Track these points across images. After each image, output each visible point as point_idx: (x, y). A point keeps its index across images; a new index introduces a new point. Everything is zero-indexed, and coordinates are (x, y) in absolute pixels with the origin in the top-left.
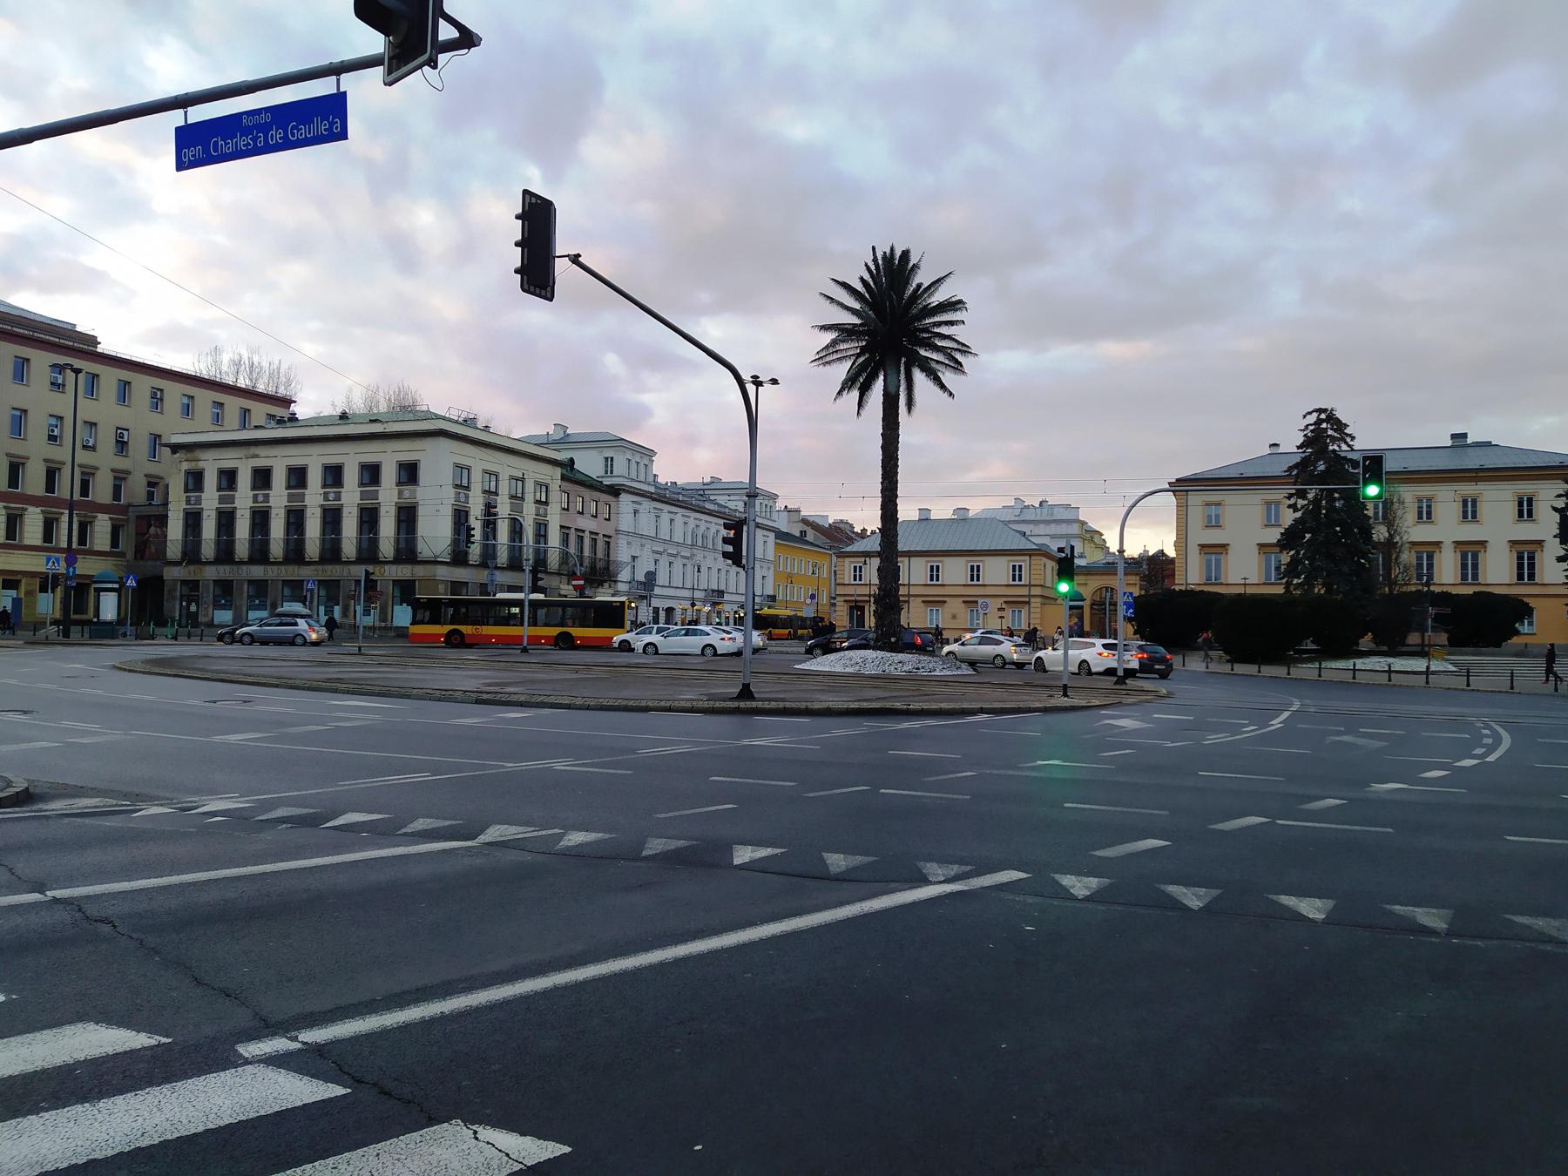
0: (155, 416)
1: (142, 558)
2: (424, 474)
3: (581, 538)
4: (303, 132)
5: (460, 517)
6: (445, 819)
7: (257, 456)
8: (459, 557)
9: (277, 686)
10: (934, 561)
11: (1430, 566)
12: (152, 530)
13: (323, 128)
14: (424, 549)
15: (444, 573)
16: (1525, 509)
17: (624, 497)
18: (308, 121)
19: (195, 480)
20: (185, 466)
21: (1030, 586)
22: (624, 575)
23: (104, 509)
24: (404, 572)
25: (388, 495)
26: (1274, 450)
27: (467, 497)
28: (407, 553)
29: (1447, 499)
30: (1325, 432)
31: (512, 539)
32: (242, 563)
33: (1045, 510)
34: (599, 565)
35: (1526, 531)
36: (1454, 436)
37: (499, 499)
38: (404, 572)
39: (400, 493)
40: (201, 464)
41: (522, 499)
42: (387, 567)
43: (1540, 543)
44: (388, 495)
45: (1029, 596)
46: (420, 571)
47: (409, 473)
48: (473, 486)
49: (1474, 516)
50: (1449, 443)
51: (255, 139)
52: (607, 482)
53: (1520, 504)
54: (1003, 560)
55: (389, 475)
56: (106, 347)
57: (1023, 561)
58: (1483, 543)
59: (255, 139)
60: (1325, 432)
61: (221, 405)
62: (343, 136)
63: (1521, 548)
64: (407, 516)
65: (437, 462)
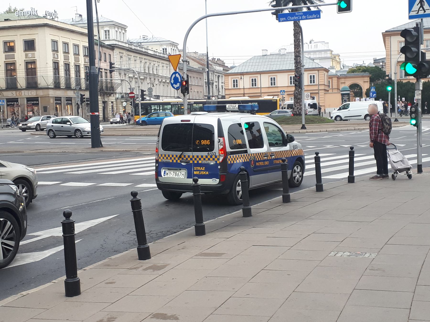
2: (37, 45)
3: (106, 73)
4: (310, 17)
5: (56, 65)
8: (57, 86)
9: (8, 152)
10: (273, 75)
13: (315, 16)
14: (41, 82)
15: (53, 93)
17: (116, 51)
18: (312, 15)
21: (319, 85)
22: (119, 90)
24: (32, 93)
27: (58, 55)
28: (32, 84)
31: (66, 74)
33: (313, 44)
34: (109, 85)
37: (70, 55)
38: (32, 93)
39: (26, 56)
41: (78, 54)
42: (23, 92)
44: (20, 57)
45: (318, 90)
46: (40, 93)
47: (30, 45)
48: (59, 50)
51: (299, 18)
52: (107, 43)
59: (299, 18)
62: (319, 18)
64: (31, 70)
65: (44, 39)
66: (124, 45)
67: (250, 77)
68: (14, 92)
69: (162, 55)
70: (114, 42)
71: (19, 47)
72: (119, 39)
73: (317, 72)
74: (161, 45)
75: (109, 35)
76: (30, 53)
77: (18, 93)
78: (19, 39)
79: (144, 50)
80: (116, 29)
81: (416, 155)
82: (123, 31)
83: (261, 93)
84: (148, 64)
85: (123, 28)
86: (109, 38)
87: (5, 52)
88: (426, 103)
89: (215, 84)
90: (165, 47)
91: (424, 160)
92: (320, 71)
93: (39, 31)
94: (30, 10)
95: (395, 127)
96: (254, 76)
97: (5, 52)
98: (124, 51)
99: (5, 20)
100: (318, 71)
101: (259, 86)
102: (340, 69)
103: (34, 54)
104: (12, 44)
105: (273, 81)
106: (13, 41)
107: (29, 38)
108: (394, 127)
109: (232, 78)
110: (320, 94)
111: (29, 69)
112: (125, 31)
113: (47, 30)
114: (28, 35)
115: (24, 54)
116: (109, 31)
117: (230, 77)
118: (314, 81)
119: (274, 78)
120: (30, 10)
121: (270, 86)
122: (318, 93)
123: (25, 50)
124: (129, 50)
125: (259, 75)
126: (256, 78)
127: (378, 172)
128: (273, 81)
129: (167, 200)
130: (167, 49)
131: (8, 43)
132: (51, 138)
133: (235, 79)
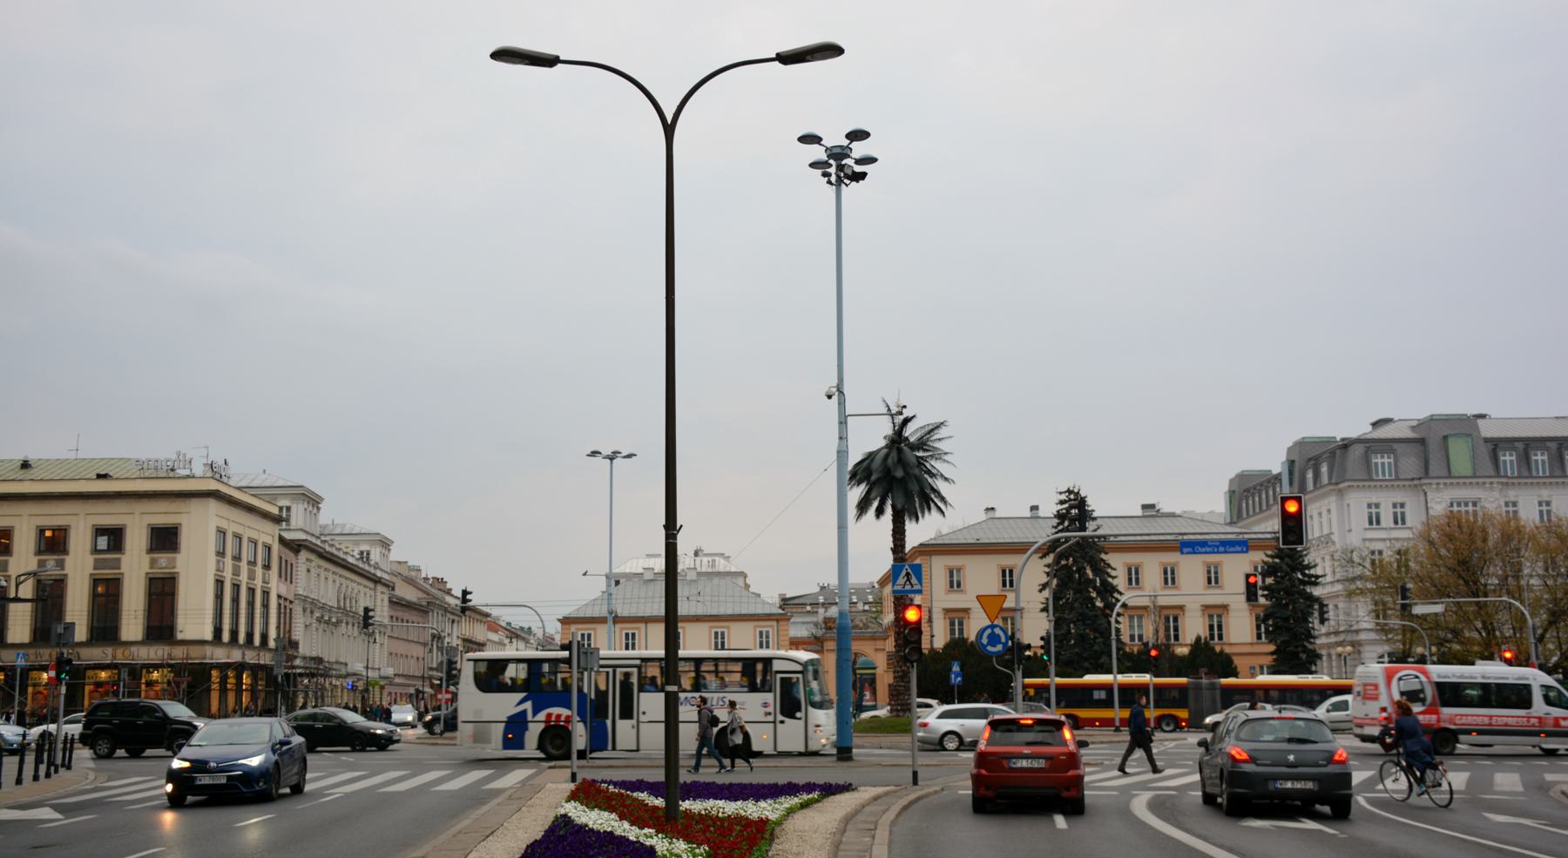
2: (185, 539)
5: (219, 583)
11: (1176, 629)
16: (1213, 579)
17: (304, 555)
26: (991, 514)
29: (1152, 567)
30: (1076, 510)
32: (81, 644)
35: (1214, 597)
36: (1144, 507)
39: (153, 563)
42: (134, 649)
43: (966, 611)
44: (135, 566)
47: (165, 539)
49: (1004, 572)
50: (1139, 512)
53: (1165, 572)
54: (705, 626)
55: (136, 540)
58: (1181, 608)
60: (1076, 510)
63: (953, 615)
64: (162, 593)
65: (201, 528)
68: (109, 651)
70: (302, 536)
71: (136, 540)
74: (357, 543)
76: (163, 558)
77: (119, 652)
78: (137, 524)
79: (341, 555)
85: (313, 501)
88: (956, 668)
90: (365, 548)
93: (195, 505)
94: (174, 457)
95: (863, 747)
98: (313, 557)
102: (208, 635)
103: (174, 560)
108: (859, 747)
113: (213, 506)
115: (146, 559)
120: (174, 457)
123: (151, 550)
125: (642, 626)
127: (963, 641)
129: (1103, 556)
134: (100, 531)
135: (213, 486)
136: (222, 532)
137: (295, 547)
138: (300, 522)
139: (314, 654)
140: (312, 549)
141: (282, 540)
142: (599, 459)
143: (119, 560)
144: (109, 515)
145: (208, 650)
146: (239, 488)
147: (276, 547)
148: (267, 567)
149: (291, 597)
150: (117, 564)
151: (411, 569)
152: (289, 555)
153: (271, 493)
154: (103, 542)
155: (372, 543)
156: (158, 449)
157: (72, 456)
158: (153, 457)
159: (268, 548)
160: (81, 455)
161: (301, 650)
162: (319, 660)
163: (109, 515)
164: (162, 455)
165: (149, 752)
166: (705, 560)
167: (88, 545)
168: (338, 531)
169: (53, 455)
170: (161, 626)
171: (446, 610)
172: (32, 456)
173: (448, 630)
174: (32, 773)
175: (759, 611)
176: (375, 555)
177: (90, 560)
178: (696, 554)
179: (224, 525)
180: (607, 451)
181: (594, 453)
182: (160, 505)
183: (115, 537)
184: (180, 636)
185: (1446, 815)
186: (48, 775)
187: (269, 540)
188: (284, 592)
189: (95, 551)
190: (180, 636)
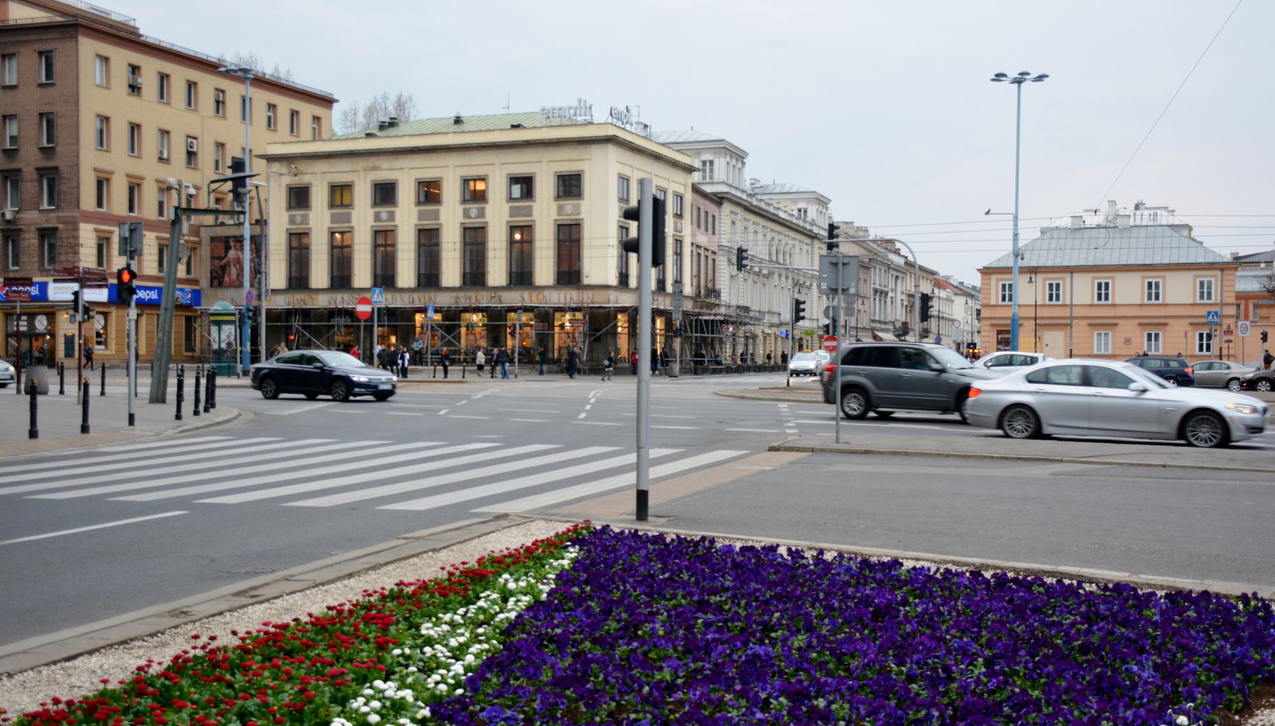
0: (218, 122)
1: (221, 285)
2: (588, 185)
6: (299, 508)
7: (374, 168)
10: (1103, 278)
12: (232, 253)
17: (727, 207)
19: (299, 197)
20: (288, 180)
23: (152, 226)
25: (545, 212)
39: (560, 209)
40: (305, 179)
42: (546, 293)
47: (570, 186)
54: (1189, 276)
55: (545, 187)
56: (151, 31)
57: (1207, 276)
61: (274, 106)
64: (569, 239)
65: (605, 178)
66: (739, 194)
67: (1196, 277)
68: (526, 294)
69: (795, 221)
70: (724, 189)
71: (545, 187)
72: (730, 182)
73: (1218, 273)
74: (795, 201)
75: (711, 171)
76: (569, 204)
77: (535, 295)
78: (406, 177)
79: (772, 210)
80: (728, 159)
81: (632, 458)
82: (740, 165)
83: (1072, 318)
84: (776, 242)
85: (738, 156)
86: (711, 178)
87: (419, 203)
89: (890, 295)
90: (802, 205)
91: (654, 472)
92: (1226, 272)
93: (596, 152)
94: (575, 104)
96: (1054, 278)
97: (419, 203)
98: (738, 210)
99: (513, 127)
100: (1222, 270)
101: (1068, 302)
103: (579, 206)
104: (480, 186)
105: (1103, 291)
106: (483, 179)
107: (567, 168)
109: (998, 280)
110: (1074, 328)
111: (517, 242)
112: (743, 163)
113: (612, 151)
114: (566, 162)
115: (554, 206)
116: (711, 162)
117: (994, 278)
118: (1209, 294)
119: (1058, 285)
120: (575, 104)
121: (1096, 302)
122: (1070, 325)
123: (558, 197)
124: (749, 209)
125: (1067, 276)
126: (1161, 281)
128: (1103, 291)
130: (809, 213)
131: (472, 183)
132: (849, 417)
133: (1054, 282)
134: (514, 180)
135: (611, 131)
136: (625, 180)
137: (719, 199)
138: (721, 177)
139: (741, 303)
140: (737, 203)
141: (696, 189)
142: (1005, 84)
143: (530, 207)
144: (521, 164)
145: (612, 295)
146: (663, 144)
147: (689, 196)
148: (679, 216)
149: (715, 249)
150: (529, 212)
151: (859, 229)
152: (712, 208)
153: (696, 147)
154: (517, 190)
155: (809, 200)
156: (564, 99)
157: (505, 111)
158: (558, 105)
159: (680, 198)
160: (511, 111)
161: (725, 298)
162: (747, 309)
163: (521, 164)
164: (564, 103)
165: (282, 396)
166: (1146, 213)
167: (504, 195)
168: (777, 190)
169: (484, 112)
170: (569, 274)
171: (889, 267)
172: (464, 114)
173: (891, 285)
174: (192, 408)
175: (1201, 260)
176: (813, 212)
177: (506, 207)
178: (1137, 207)
179: (627, 172)
180: (1013, 74)
181: (999, 77)
182: (555, 153)
183: (526, 184)
184: (586, 281)
185: (391, 131)
186: (206, 410)
187: (681, 190)
188: (703, 239)
189: (511, 199)
190: (586, 281)
